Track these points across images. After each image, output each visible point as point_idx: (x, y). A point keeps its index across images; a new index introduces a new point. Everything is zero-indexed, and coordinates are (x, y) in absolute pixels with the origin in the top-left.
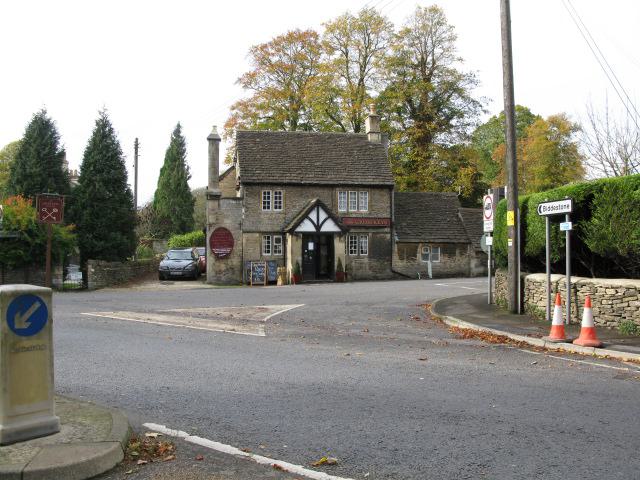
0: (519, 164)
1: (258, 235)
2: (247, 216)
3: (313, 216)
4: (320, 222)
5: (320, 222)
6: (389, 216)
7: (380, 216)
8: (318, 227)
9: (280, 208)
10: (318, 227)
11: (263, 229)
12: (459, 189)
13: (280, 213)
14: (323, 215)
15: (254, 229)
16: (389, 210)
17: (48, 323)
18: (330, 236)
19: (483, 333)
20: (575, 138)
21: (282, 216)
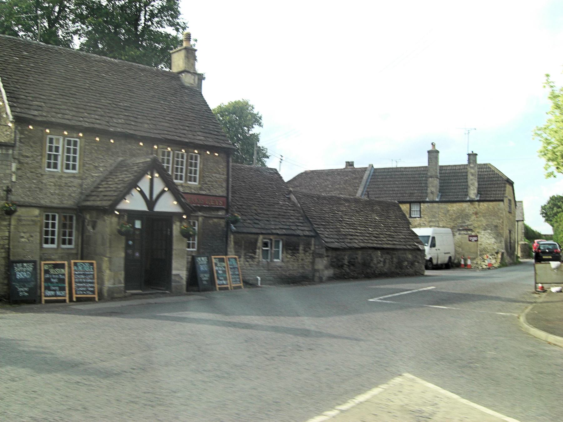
0: (190, 333)
1: (37, 212)
2: (19, 177)
3: (144, 184)
4: (155, 196)
5: (155, 196)
6: (224, 194)
7: (214, 192)
8: (151, 203)
9: (74, 168)
10: (151, 203)
11: (46, 202)
12: (106, 259)
13: (74, 176)
14: (159, 186)
15: (30, 200)
16: (224, 185)
17: (4, 311)
18: (168, 218)
19: (294, 202)
20: (256, 130)
21: (77, 181)
